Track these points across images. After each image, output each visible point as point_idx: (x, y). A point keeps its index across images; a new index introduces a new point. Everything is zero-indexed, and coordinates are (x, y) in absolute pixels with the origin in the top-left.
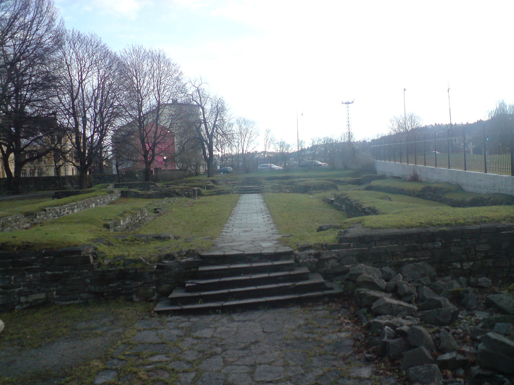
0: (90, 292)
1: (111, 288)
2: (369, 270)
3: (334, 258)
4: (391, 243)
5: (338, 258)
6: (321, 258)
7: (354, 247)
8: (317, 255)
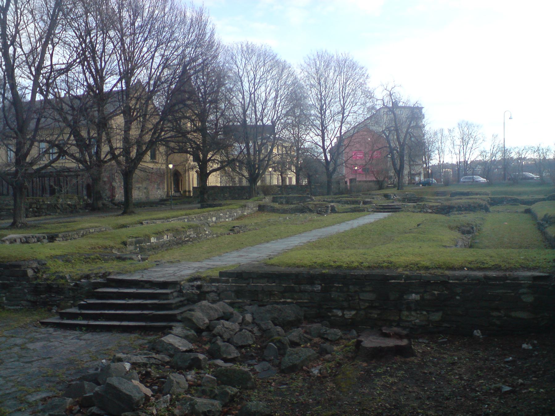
0: (27, 301)
1: (41, 298)
2: (203, 307)
3: (213, 291)
4: (268, 282)
5: (218, 292)
6: (202, 290)
7: (232, 283)
8: (199, 287)
